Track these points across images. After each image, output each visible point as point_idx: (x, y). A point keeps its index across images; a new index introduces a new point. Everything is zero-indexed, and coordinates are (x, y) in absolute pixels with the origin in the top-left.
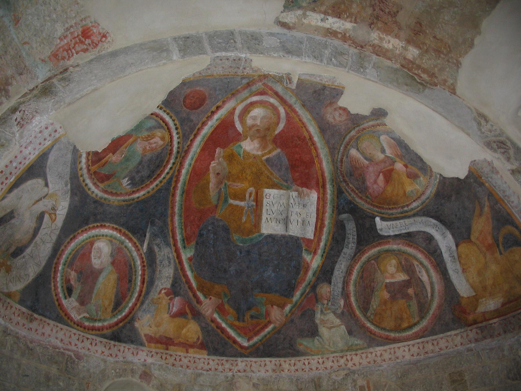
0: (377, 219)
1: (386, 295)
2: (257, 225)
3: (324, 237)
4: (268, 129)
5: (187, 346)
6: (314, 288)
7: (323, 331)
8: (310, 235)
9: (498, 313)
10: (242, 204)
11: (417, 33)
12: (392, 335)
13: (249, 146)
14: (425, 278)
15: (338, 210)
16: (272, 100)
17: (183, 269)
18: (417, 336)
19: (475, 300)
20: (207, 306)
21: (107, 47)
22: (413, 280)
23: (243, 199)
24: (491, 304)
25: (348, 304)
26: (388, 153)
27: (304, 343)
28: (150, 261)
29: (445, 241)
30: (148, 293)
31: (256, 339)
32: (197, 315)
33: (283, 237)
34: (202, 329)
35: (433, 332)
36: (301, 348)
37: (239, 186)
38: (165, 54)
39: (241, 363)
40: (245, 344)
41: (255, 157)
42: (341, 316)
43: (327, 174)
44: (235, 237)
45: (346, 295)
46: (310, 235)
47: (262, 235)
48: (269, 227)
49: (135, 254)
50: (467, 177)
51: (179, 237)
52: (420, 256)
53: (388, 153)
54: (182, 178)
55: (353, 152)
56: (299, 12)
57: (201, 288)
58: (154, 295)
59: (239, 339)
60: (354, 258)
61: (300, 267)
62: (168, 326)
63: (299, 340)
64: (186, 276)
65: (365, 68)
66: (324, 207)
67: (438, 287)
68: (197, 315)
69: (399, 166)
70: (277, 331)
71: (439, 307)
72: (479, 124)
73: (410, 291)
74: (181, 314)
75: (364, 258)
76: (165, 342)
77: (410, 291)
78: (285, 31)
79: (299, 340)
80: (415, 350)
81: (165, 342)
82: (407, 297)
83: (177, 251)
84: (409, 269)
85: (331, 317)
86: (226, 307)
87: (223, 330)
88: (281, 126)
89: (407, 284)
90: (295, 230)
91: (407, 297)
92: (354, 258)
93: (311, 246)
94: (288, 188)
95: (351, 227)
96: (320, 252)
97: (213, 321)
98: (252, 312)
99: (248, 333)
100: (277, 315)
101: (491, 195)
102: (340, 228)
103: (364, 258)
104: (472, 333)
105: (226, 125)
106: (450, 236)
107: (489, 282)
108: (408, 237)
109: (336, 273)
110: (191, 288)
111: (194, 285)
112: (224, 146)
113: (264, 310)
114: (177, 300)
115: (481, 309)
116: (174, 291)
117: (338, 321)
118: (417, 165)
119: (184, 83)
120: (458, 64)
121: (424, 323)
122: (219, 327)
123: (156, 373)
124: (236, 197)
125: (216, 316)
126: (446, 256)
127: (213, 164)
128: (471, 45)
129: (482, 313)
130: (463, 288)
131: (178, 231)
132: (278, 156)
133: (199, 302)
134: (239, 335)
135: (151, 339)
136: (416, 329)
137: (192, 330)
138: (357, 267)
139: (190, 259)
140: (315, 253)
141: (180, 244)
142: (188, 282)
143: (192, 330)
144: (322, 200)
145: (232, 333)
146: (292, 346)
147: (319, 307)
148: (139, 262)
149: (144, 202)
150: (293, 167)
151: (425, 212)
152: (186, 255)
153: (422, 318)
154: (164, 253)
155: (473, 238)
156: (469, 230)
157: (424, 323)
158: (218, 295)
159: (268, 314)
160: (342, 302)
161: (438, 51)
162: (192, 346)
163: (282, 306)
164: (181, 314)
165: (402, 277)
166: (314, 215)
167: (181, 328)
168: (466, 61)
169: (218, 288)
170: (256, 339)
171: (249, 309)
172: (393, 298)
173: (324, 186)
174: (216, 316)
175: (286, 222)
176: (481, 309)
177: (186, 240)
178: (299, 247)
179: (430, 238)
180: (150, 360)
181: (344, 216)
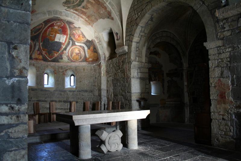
0: (76, 42)
1: (75, 54)
2: (54, 39)
3: (66, 43)
4: (60, 26)
5: (40, 60)
6: (63, 51)
7: (64, 58)
8: (64, 42)
9: (91, 61)
10: (52, 36)
11: (88, 17)
12: (75, 61)
13: (56, 27)
14: (82, 53)
15: (69, 39)
16: (62, 22)
17: (40, 46)
18: (79, 62)
19: (89, 58)
20: (44, 53)
21: (36, 13)
22: (80, 53)
23: (52, 35)
24: (91, 59)
25: (68, 55)
26: (80, 33)
27: (60, 60)
28: (35, 45)
29: (86, 48)
30: (34, 50)
31: (52, 59)
32: (42, 54)
33: (59, 42)
34: (43, 57)
35: (82, 62)
36: (59, 61)
37: (52, 33)
38: (45, 15)
39: (49, 63)
40: (50, 60)
41: (56, 29)
42: (67, 56)
43: (69, 34)
44: (50, 41)
45: (68, 53)
46: (64, 42)
47: (55, 41)
48: (56, 40)
49: (33, 44)
50: (91, 41)
51: (40, 41)
52: (82, 49)
53: (80, 33)
54: (43, 31)
55: (74, 31)
56: (70, 9)
57: (43, 50)
58: (35, 51)
59: (49, 59)
60: (71, 47)
61: (61, 47)
62: (37, 56)
63: (59, 60)
64: (40, 47)
65: (78, 20)
66: (67, 38)
67: (84, 55)
68: (42, 54)
69: (81, 35)
70: (56, 58)
71: (83, 58)
72: (95, 33)
73: (79, 55)
74: (39, 54)
75: (72, 48)
76: (36, 59)
77: (79, 55)
78: (66, 11)
79: (59, 60)
80: (78, 64)
81: (36, 59)
82: (78, 55)
83: (40, 43)
84: (80, 51)
85: (65, 56)
86: (47, 53)
87: (46, 57)
88: (62, 26)
89: (79, 53)
90: (61, 41)
91: (78, 55)
92: (71, 47)
93: (63, 44)
94: (61, 34)
95: (71, 42)
96: (65, 45)
97: (45, 55)
98: (52, 54)
99: (50, 58)
100: (56, 55)
101: (94, 44)
102: (69, 42)
103: (72, 48)
104: (87, 63)
105: (53, 24)
106: (87, 48)
107: (91, 56)
108: (80, 46)
109: (67, 49)
110: (41, 50)
111: (42, 49)
112: (51, 27)
113: (53, 54)
114: (39, 52)
115: (89, 60)
116: (38, 50)
117: (66, 57)
118: (84, 36)
119: (48, 19)
120: (94, 23)
121: (80, 60)
122: (45, 56)
123: (35, 64)
124: (51, 34)
125: (45, 55)
126: (86, 50)
127: (49, 29)
128: (96, 22)
129: (88, 49)
130: (87, 56)
131: (40, 40)
132: (61, 30)
133: (42, 52)
134: (49, 58)
135: (34, 59)
136: (79, 61)
137: (41, 57)
138: (71, 49)
139: (42, 45)
140: (64, 45)
141: (40, 42)
142: (41, 48)
143: (41, 57)
144: (67, 37)
145: (48, 58)
146: (58, 61)
147: (63, 54)
148: (33, 45)
149: (35, 36)
150: (63, 31)
151: (84, 43)
152: (41, 44)
153: (80, 59)
154: (37, 44)
155: (90, 49)
156: (90, 48)
157: (80, 60)
158: (46, 51)
159: (54, 55)
160: (67, 54)
161: (91, 21)
162: (41, 60)
163: (57, 53)
164: (39, 54)
165: (78, 52)
166: (65, 39)
167: (39, 56)
168: (95, 23)
169: (46, 50)
170: (52, 59)
171: (51, 53)
172: (76, 55)
173: (68, 35)
174: (45, 55)
175: (60, 40)
176: (89, 60)
177: (41, 41)
178: (61, 44)
179: (84, 47)
180: (34, 62)
181: (70, 40)
